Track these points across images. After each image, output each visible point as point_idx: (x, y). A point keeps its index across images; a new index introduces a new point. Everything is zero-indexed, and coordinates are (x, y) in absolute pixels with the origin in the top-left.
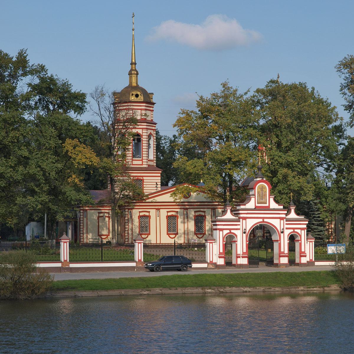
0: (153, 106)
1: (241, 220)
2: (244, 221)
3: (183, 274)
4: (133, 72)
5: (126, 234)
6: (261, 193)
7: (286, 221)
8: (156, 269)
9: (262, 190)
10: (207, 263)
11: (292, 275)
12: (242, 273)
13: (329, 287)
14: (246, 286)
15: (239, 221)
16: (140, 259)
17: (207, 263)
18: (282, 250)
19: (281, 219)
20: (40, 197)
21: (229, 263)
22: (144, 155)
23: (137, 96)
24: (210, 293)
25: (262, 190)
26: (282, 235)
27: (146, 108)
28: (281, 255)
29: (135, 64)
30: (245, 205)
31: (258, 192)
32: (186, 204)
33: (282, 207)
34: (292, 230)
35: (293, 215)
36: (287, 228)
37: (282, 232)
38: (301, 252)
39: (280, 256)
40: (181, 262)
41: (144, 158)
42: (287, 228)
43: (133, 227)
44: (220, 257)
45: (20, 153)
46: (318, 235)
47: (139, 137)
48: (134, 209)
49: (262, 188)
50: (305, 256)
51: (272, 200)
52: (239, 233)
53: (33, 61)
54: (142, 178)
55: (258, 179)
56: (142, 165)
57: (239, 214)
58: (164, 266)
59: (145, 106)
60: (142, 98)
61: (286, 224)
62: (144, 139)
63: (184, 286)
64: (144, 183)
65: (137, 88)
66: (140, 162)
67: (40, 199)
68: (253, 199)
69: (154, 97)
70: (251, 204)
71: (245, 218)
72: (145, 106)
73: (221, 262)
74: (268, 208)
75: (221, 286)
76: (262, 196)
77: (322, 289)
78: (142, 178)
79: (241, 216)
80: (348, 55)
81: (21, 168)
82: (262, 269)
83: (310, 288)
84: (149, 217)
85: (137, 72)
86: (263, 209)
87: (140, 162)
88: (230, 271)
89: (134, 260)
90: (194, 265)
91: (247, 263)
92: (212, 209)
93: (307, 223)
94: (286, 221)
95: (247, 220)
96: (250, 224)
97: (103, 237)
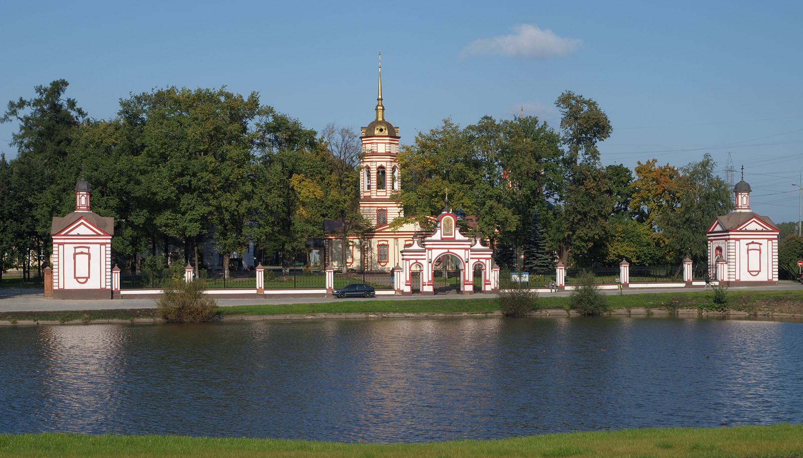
0: (398, 140)
1: (427, 250)
2: (430, 252)
3: (354, 301)
4: (379, 108)
5: (366, 262)
6: (447, 226)
7: (471, 251)
8: (341, 296)
9: (448, 223)
10: (394, 290)
11: (417, 302)
12: (456, 298)
13: (492, 313)
14: (409, 312)
15: (425, 252)
16: (330, 286)
17: (394, 290)
18: (467, 279)
19: (466, 249)
20: (265, 229)
21: (415, 291)
22: (388, 187)
23: (381, 130)
24: (372, 318)
25: (448, 223)
26: (467, 264)
27: (390, 142)
28: (466, 283)
29: (382, 100)
30: (431, 237)
31: (444, 225)
32: (424, 233)
33: (467, 238)
34: (477, 260)
35: (478, 246)
36: (471, 258)
37: (467, 262)
38: (486, 280)
39: (465, 284)
40: (364, 290)
41: (387, 189)
42: (471, 258)
43: (373, 255)
44: (406, 285)
45: (244, 188)
46: (543, 263)
47: (384, 170)
48: (373, 238)
49: (448, 221)
50: (490, 284)
51: (457, 231)
52: (425, 263)
53: (263, 103)
54: (385, 209)
55: (444, 213)
56: (386, 196)
57: (425, 245)
58: (348, 293)
59: (389, 140)
60: (387, 132)
61: (471, 254)
62: (388, 172)
63: (348, 311)
64: (388, 214)
65: (383, 122)
66: (384, 194)
67: (264, 231)
68: (439, 231)
69: (455, 122)
70: (437, 236)
71: (430, 249)
72: (389, 140)
73: (407, 289)
74: (453, 240)
75: (385, 312)
76: (448, 228)
77: (485, 315)
78: (385, 209)
79: (427, 246)
80: (566, 91)
81: (245, 202)
82: (452, 296)
83: (473, 313)
84: (388, 245)
85: (383, 107)
86: (451, 240)
87: (384, 194)
88: (415, 297)
89: (325, 287)
90: (377, 293)
91: (472, 290)
92: (395, 238)
93: (492, 253)
94: (471, 251)
95: (433, 250)
96: (436, 254)
97: (348, 265)
